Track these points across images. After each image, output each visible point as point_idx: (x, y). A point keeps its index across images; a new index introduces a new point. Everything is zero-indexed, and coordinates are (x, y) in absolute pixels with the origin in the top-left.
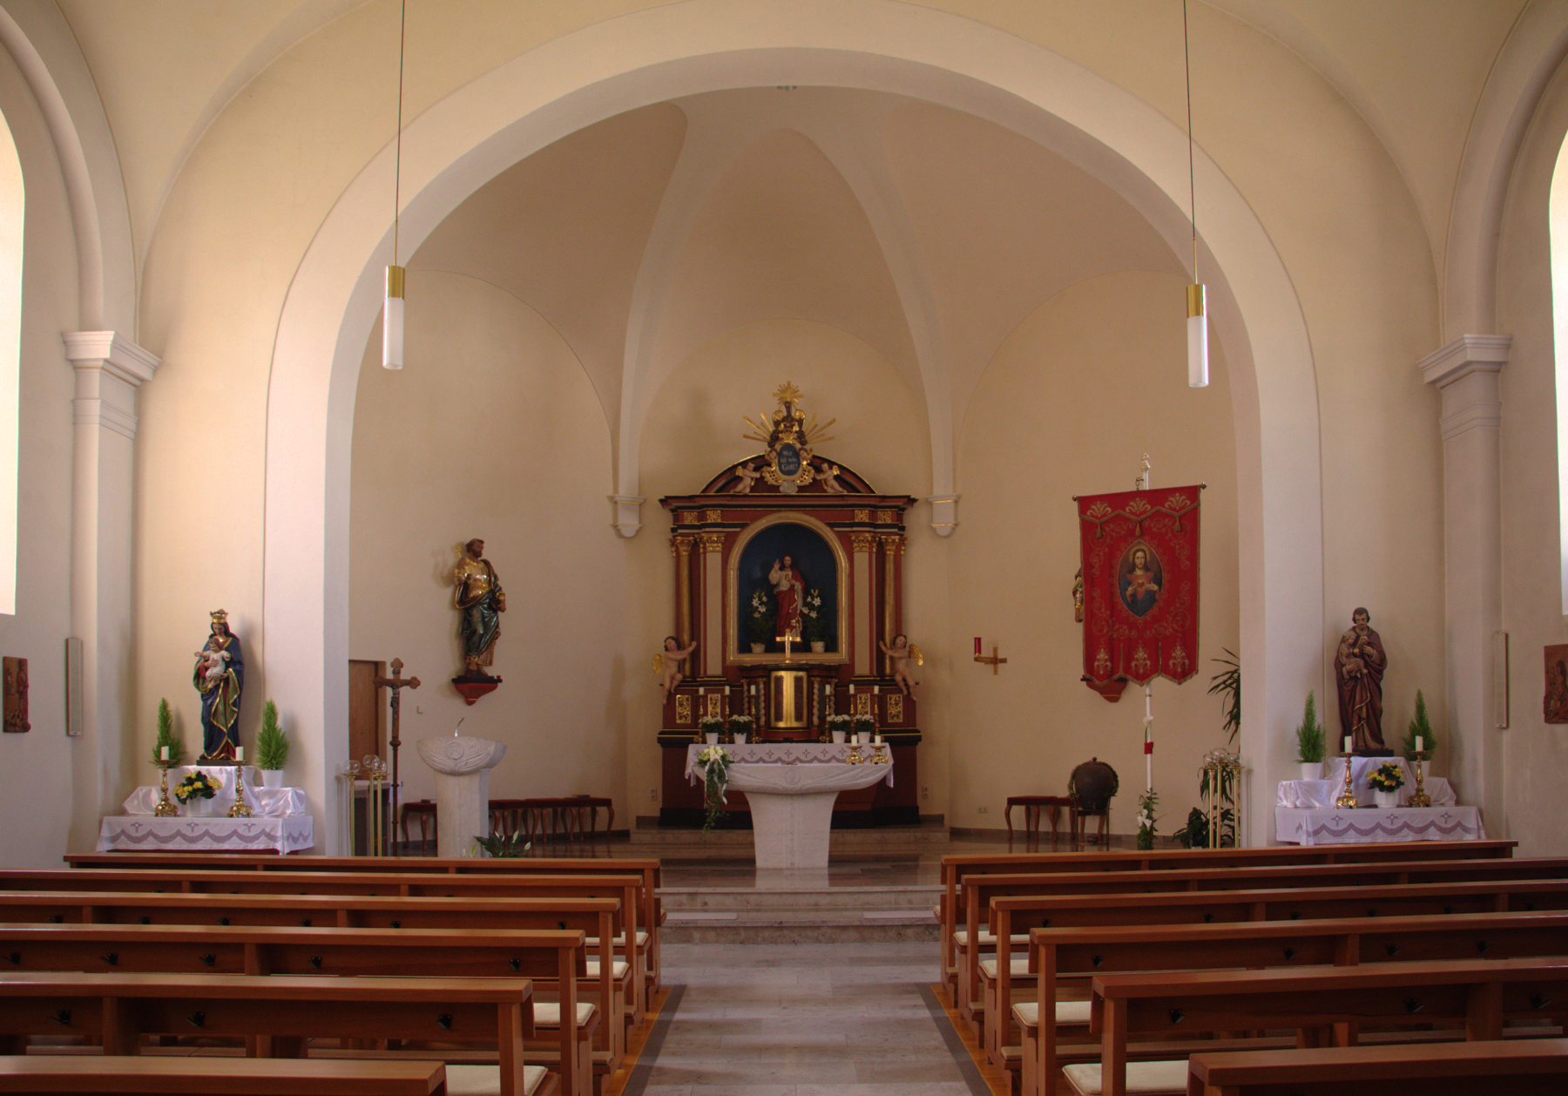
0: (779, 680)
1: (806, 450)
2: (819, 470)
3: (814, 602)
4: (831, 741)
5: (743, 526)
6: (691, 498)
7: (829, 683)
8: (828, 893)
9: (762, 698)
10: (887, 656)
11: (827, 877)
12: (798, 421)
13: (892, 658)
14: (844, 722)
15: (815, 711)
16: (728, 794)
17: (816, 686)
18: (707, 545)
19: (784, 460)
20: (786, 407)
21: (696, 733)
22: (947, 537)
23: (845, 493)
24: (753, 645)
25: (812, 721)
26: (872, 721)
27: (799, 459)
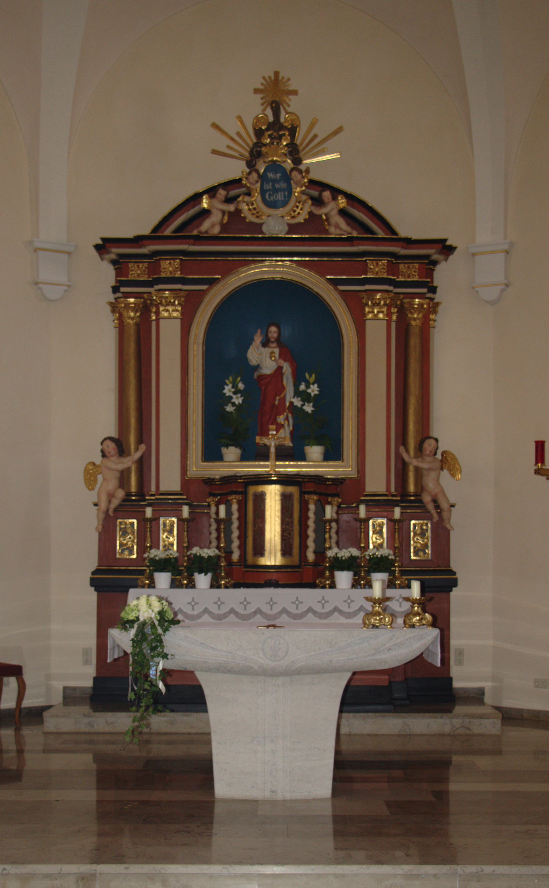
0: (260, 499)
1: (300, 172)
2: (318, 202)
3: (309, 391)
4: (333, 586)
5: (212, 282)
6: (138, 240)
7: (329, 503)
8: (232, 139)
9: (236, 524)
10: (411, 468)
11: (330, 827)
12: (289, 130)
13: (418, 470)
14: (352, 558)
15: (311, 543)
16: (166, 674)
17: (312, 507)
18: (161, 308)
19: (268, 186)
20: (272, 108)
21: (142, 572)
22: (492, 303)
23: (355, 234)
24: (224, 450)
25: (306, 557)
26: (392, 557)
27: (290, 185)
